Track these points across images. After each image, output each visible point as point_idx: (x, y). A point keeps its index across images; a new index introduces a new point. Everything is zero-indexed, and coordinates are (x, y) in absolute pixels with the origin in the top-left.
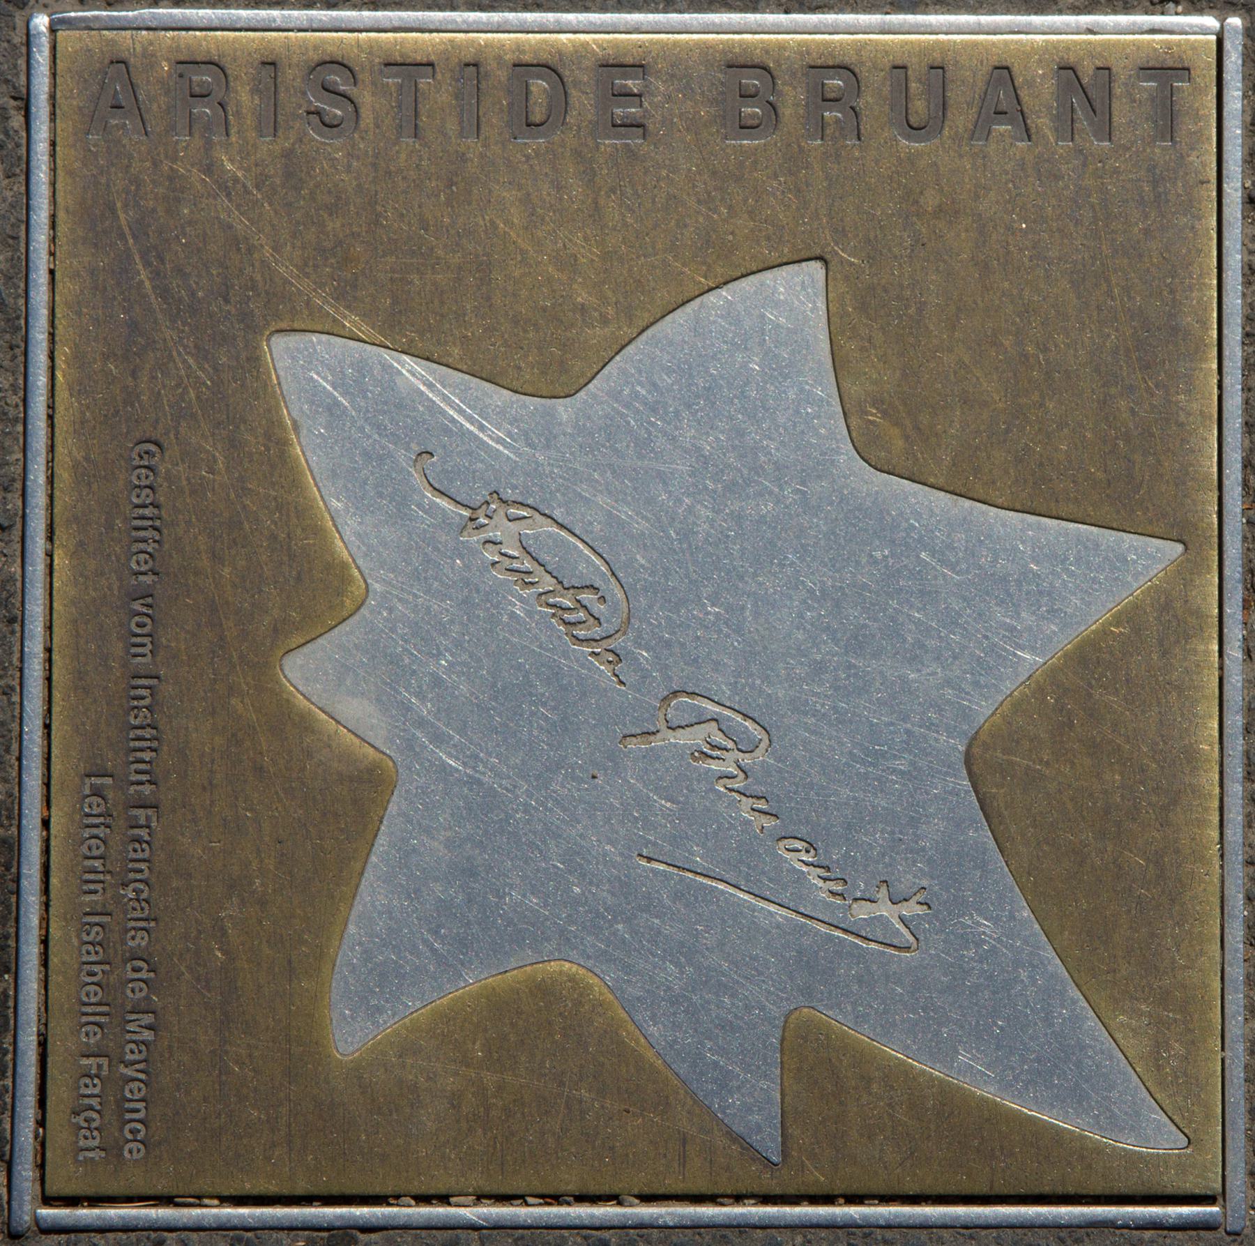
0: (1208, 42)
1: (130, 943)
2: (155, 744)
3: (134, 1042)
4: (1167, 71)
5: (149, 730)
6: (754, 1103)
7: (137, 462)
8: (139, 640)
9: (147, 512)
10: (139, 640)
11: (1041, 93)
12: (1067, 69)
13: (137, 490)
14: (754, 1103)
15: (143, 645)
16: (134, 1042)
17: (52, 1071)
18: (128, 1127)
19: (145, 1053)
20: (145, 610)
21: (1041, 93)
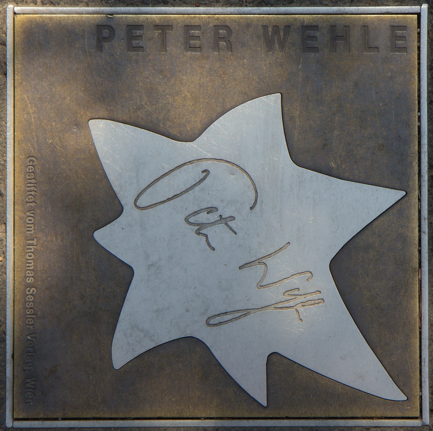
0: (412, 19)
1: (28, 282)
2: (35, 185)
3: (29, 270)
4: (397, 30)
5: (33, 180)
6: (255, 384)
7: (29, 164)
8: (29, 261)
9: (33, 181)
10: (29, 261)
11: (383, 40)
12: (333, 27)
13: (28, 174)
14: (255, 384)
15: (31, 227)
16: (29, 270)
17: (15, 178)
18: (28, 255)
19: (33, 273)
20: (33, 215)
21: (383, 40)
